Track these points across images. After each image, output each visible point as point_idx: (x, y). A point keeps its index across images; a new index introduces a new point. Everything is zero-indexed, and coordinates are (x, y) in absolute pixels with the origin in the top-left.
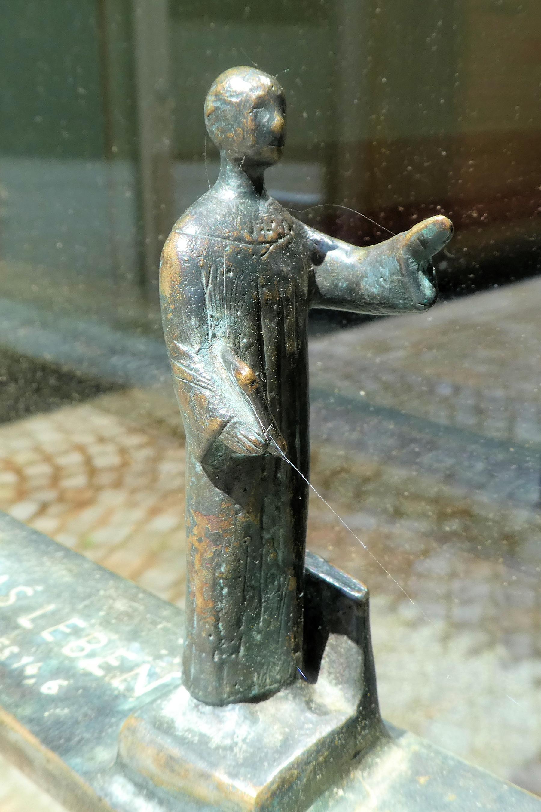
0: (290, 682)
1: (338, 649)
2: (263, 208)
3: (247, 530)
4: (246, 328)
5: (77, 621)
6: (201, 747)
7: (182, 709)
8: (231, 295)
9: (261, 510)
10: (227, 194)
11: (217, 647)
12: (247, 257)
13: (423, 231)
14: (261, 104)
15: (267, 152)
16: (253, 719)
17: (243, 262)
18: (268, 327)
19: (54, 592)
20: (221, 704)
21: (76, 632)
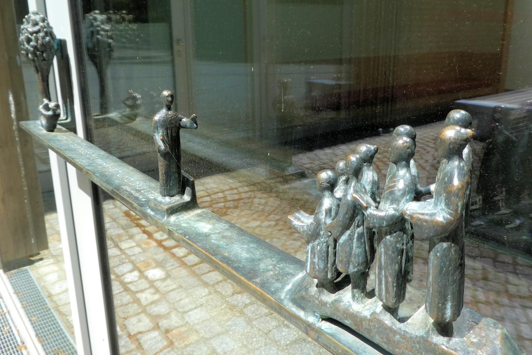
0: (178, 193)
1: (188, 190)
2: (170, 113)
3: (167, 165)
4: (165, 131)
5: (153, 192)
6: (161, 203)
7: (160, 198)
8: (162, 126)
9: (170, 162)
10: (164, 111)
11: (164, 186)
12: (165, 120)
13: (313, 94)
14: (167, 96)
15: (170, 104)
16: (170, 199)
17: (164, 121)
18: (169, 132)
19: (150, 187)
20: (165, 196)
21: (152, 193)
